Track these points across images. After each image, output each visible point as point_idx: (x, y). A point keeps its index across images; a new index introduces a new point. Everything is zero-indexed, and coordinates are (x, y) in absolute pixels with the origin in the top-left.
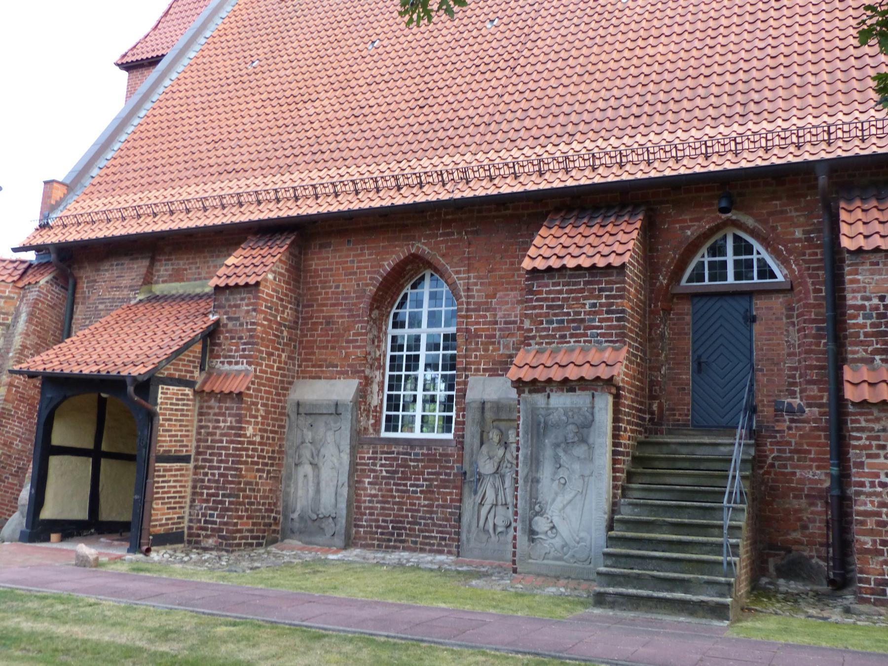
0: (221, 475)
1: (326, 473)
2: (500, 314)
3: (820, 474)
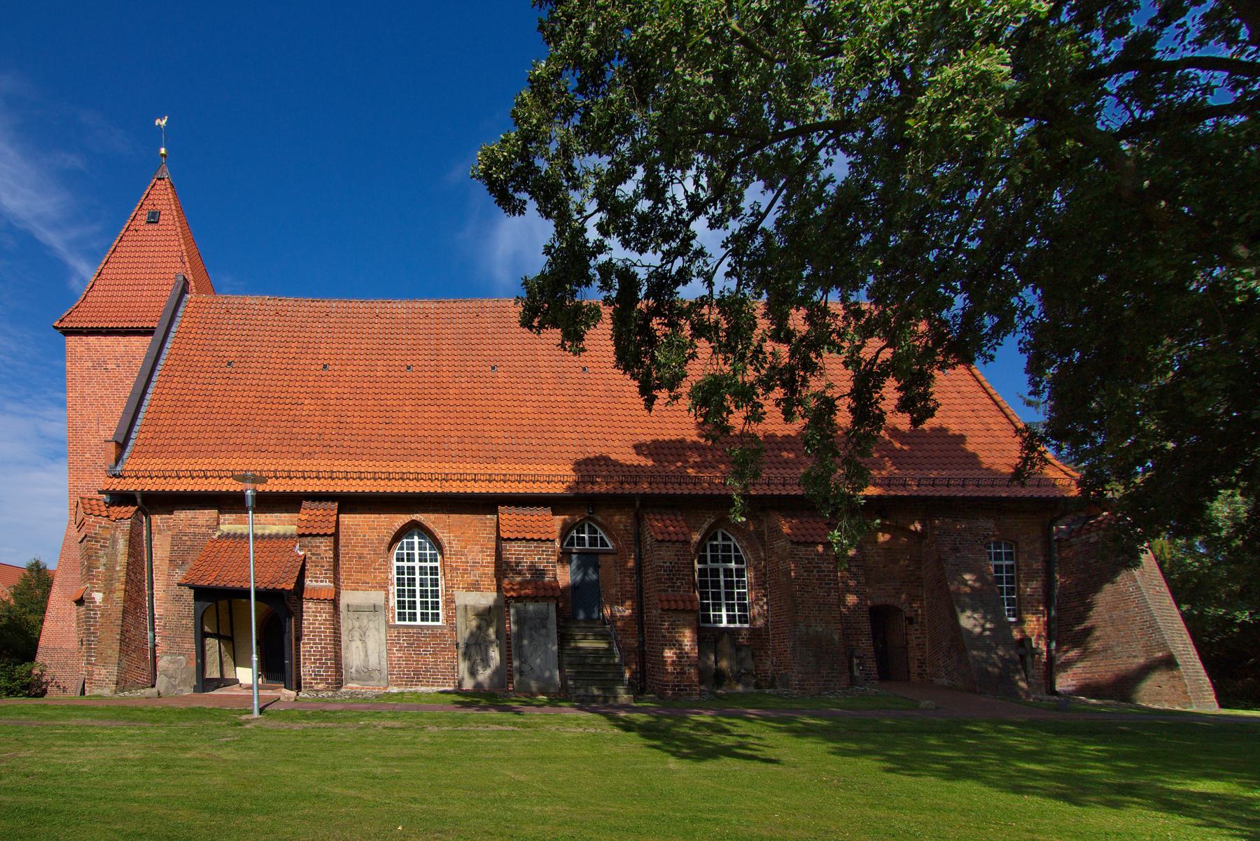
1: (372, 645)
2: (470, 557)
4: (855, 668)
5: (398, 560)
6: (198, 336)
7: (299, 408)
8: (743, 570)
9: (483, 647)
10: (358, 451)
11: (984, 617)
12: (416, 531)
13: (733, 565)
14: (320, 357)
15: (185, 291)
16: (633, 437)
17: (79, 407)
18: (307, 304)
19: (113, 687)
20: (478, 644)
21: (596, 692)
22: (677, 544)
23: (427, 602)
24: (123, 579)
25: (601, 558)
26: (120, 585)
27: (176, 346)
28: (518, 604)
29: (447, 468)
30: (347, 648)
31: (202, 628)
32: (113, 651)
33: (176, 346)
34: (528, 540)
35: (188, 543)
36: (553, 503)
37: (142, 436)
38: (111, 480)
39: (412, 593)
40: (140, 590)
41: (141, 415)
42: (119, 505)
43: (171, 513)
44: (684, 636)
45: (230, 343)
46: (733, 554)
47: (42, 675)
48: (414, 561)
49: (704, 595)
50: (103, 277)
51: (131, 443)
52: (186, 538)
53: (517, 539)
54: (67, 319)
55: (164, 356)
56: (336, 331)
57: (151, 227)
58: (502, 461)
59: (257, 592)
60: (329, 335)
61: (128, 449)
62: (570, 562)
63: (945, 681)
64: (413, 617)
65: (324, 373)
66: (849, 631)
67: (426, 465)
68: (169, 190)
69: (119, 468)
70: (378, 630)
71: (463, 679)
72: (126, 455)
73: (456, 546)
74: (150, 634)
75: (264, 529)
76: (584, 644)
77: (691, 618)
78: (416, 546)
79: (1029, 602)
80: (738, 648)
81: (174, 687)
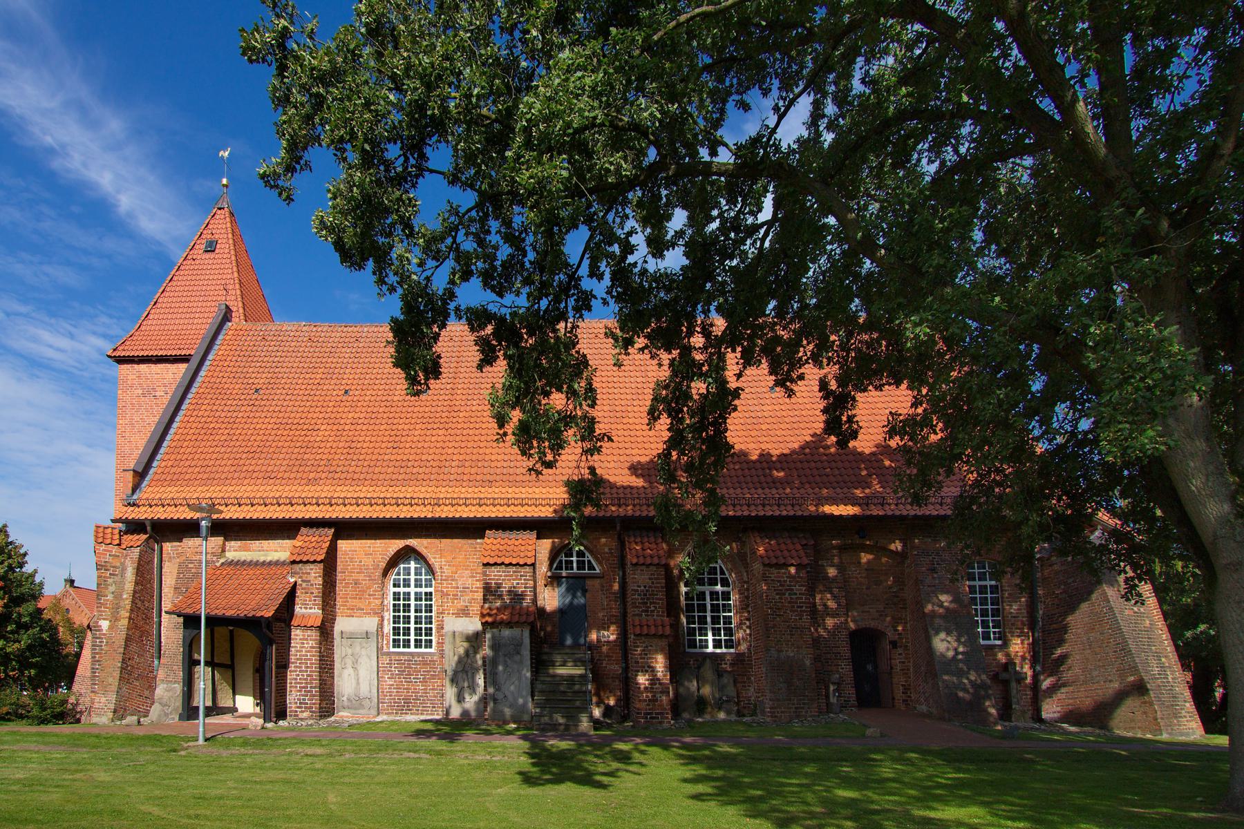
0: (308, 675)
3: (617, 667)
4: (831, 696)
5: (395, 586)
6: (232, 364)
7: (315, 433)
8: (729, 593)
9: (470, 674)
10: (362, 476)
11: (958, 640)
12: (413, 556)
13: (719, 588)
14: (344, 382)
15: (227, 316)
16: (628, 459)
17: (127, 434)
18: (340, 329)
19: (111, 715)
20: (464, 671)
21: (561, 721)
22: (651, 567)
23: (421, 629)
24: (128, 607)
25: (589, 582)
26: (125, 614)
27: (211, 373)
28: (495, 630)
29: (443, 493)
30: (340, 676)
32: (113, 679)
33: (211, 373)
34: (507, 565)
35: (193, 570)
36: (540, 527)
37: (164, 464)
38: (126, 508)
39: (407, 620)
40: (148, 618)
41: (165, 444)
42: (132, 534)
43: (180, 540)
44: (656, 662)
45: (261, 370)
46: (719, 577)
47: (77, 704)
49: (690, 620)
50: (158, 305)
51: (152, 471)
53: (496, 564)
54: (121, 348)
55: (196, 384)
56: (363, 355)
57: (208, 255)
58: (497, 484)
59: (208, 618)
60: (356, 360)
61: (148, 478)
62: (559, 585)
63: (924, 708)
64: (407, 644)
65: (344, 398)
66: (829, 656)
67: (423, 489)
68: (228, 219)
69: (135, 497)
70: (369, 657)
71: (450, 706)
72: (145, 483)
73: (447, 571)
75: (266, 555)
76: (561, 671)
77: (664, 643)
79: (1013, 624)
80: (720, 674)
81: (166, 715)
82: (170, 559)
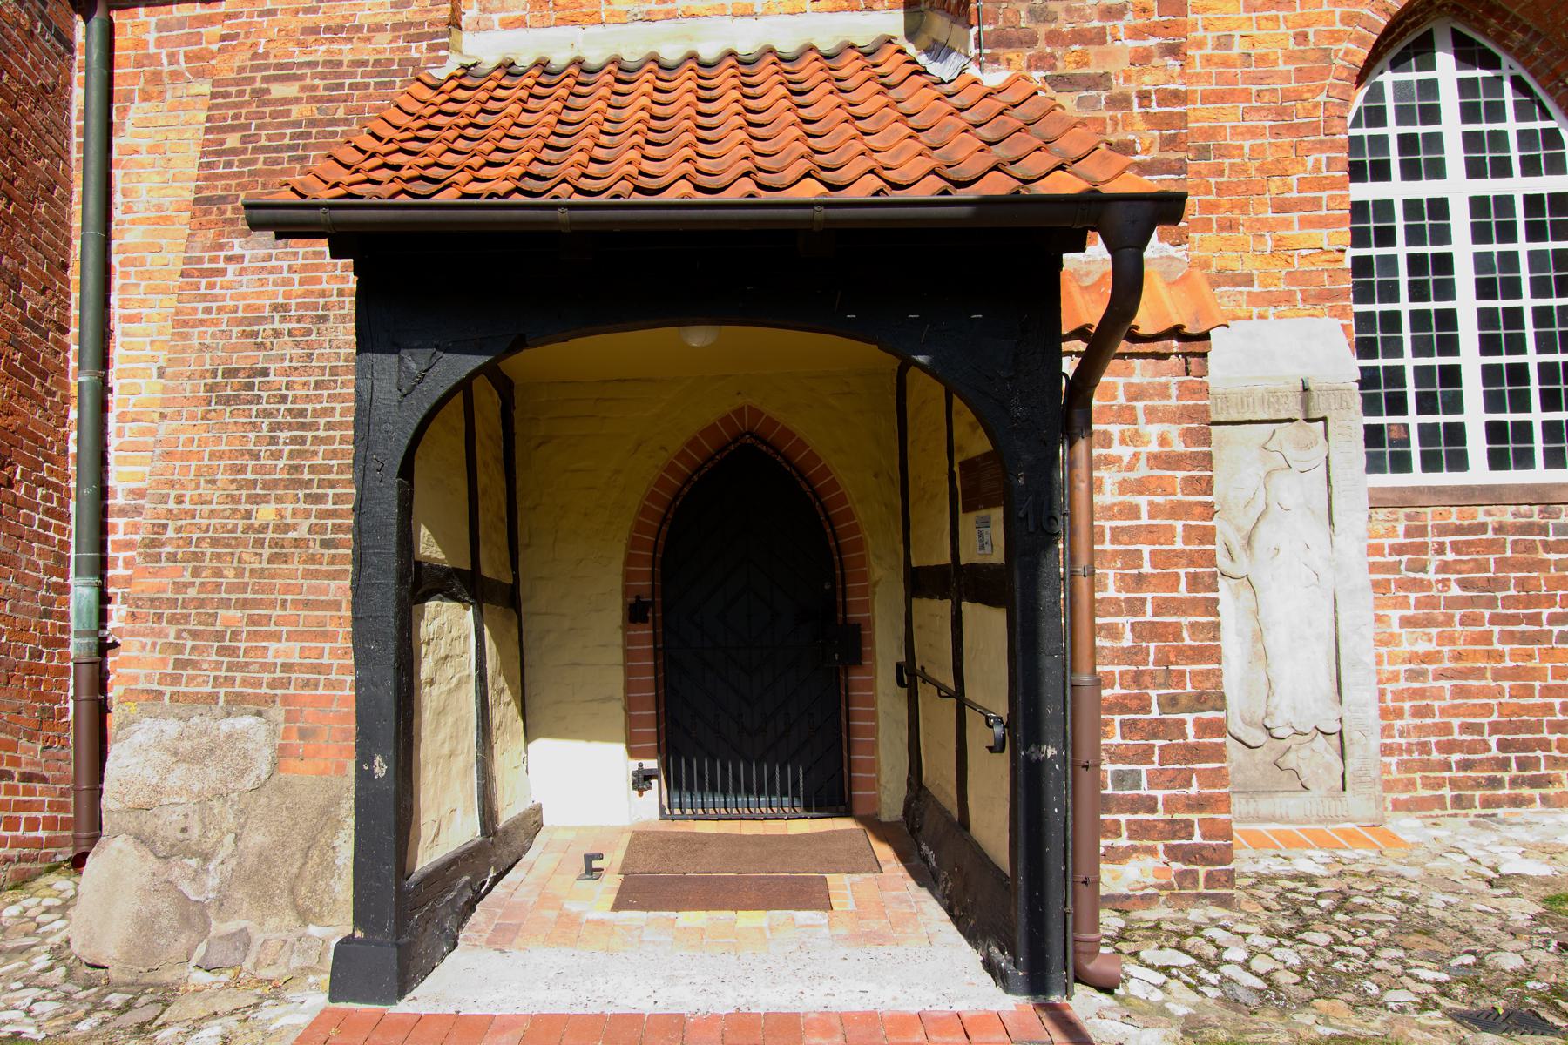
31: (407, 540)
35: (296, 112)
48: (1437, 170)
52: (291, 90)
74: (81, 592)
78: (1449, 101)
82: (155, 86)
